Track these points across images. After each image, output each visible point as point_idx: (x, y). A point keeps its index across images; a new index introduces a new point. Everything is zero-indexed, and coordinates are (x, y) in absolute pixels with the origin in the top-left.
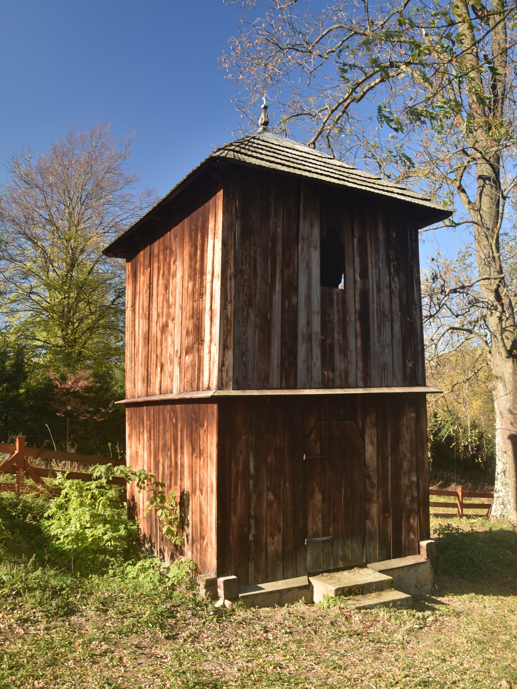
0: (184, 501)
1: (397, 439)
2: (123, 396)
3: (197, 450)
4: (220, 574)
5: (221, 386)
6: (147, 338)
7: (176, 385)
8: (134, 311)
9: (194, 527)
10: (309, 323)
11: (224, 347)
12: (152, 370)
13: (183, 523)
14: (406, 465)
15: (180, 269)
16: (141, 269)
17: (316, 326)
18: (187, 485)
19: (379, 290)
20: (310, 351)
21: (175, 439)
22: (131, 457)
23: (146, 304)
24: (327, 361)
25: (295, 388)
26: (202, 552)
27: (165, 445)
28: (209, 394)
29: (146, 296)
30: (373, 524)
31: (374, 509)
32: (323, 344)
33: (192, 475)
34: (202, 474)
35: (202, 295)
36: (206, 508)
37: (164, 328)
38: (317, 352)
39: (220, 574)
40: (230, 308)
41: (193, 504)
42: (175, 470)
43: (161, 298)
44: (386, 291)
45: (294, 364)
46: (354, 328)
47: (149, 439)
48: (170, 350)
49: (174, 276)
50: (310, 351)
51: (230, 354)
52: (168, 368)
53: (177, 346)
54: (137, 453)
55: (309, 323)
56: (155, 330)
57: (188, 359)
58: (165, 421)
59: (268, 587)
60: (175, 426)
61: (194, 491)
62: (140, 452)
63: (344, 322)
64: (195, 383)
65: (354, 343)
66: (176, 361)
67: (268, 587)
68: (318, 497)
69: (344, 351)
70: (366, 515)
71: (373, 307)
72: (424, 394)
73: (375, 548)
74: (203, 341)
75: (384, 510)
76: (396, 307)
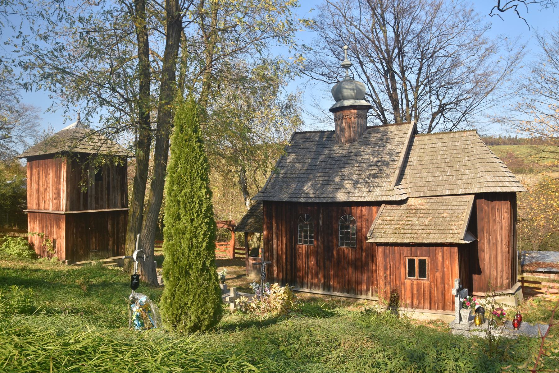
0: (54, 241)
1: (118, 223)
2: (26, 208)
3: (58, 227)
4: (66, 259)
5: (66, 211)
6: (38, 191)
7: (51, 208)
8: (31, 180)
9: (58, 248)
10: (91, 192)
11: (67, 200)
12: (41, 202)
13: (54, 247)
14: (121, 230)
15: (51, 176)
16: (34, 167)
17: (94, 193)
18: (55, 237)
19: (113, 181)
20: (91, 200)
21: (51, 224)
22: (31, 229)
23: (37, 179)
24: (97, 203)
25: (87, 210)
26: (61, 254)
27: (46, 226)
28: (63, 213)
29: (37, 177)
30: (110, 247)
31: (111, 243)
32: (95, 198)
33: (57, 234)
34: (60, 235)
35: (60, 184)
36: (62, 243)
37: (45, 190)
38: (94, 200)
39: (66, 259)
40: (69, 190)
41: (58, 242)
42: (50, 233)
43: (44, 180)
44: (116, 181)
45: (87, 204)
46: (105, 192)
47: (40, 223)
48: (48, 197)
49: (49, 174)
50: (91, 200)
51: (69, 202)
52: (47, 202)
53: (51, 196)
54: (34, 228)
55: (91, 192)
56: (42, 189)
57: (55, 201)
58: (46, 218)
59: (79, 263)
60: (51, 220)
61: (58, 238)
62: (35, 228)
63: (102, 191)
64: (58, 208)
65: (105, 197)
66: (50, 201)
67: (79, 263)
68: (94, 239)
69: (102, 199)
70: (108, 244)
71: (111, 186)
72: (127, 210)
73: (110, 253)
74: (60, 197)
75: (114, 243)
76: (119, 185)
